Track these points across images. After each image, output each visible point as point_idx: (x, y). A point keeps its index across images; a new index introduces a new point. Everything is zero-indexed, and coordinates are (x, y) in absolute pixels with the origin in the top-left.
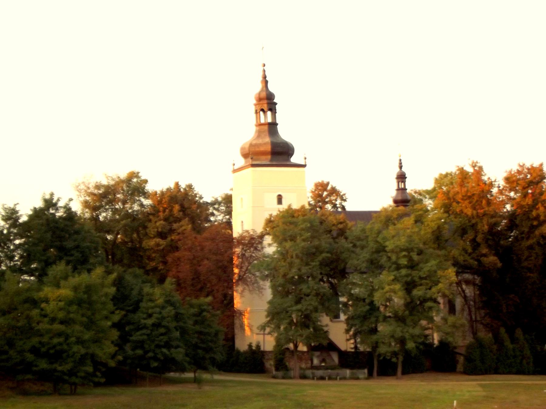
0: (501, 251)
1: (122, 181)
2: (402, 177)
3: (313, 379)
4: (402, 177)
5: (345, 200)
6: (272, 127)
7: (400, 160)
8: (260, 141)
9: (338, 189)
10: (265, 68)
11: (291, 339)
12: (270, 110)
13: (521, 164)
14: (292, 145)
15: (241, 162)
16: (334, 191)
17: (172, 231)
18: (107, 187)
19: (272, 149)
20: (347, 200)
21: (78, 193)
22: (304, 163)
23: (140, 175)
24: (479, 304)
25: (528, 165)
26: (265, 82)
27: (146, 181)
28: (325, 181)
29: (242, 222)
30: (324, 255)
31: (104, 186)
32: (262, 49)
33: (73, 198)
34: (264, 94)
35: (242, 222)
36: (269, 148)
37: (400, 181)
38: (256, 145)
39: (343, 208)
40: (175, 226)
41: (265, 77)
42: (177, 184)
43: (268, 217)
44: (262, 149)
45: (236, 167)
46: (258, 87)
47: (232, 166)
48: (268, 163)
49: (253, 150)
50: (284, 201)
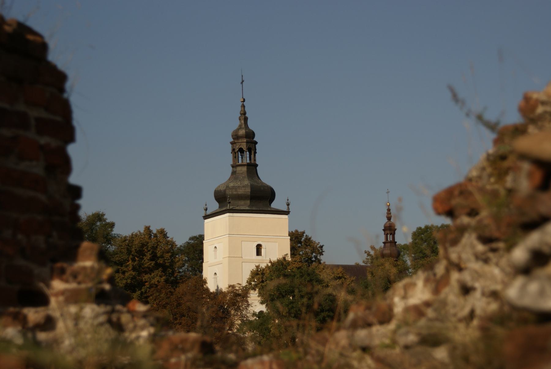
6: (252, 167)
9: (314, 240)
10: (244, 103)
20: (323, 253)
22: (285, 208)
27: (112, 225)
28: (300, 230)
32: (452, 90)
34: (242, 132)
36: (248, 190)
37: (389, 233)
40: (146, 277)
41: (244, 113)
42: (148, 229)
43: (255, 269)
44: (241, 192)
45: (209, 212)
46: (235, 124)
47: (204, 212)
48: (247, 208)
49: (230, 193)
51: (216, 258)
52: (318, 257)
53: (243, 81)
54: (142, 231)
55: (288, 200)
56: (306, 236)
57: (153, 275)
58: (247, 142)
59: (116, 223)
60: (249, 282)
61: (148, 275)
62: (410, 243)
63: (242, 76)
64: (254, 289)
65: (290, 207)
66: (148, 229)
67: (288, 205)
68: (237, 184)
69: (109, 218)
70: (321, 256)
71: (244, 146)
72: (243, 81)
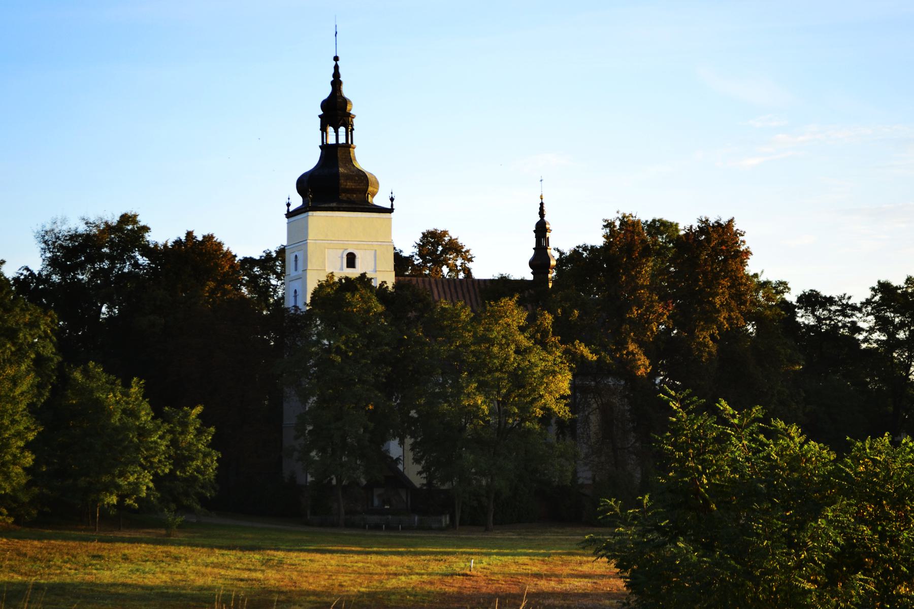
0: (198, 409)
1: (109, 228)
2: (541, 230)
3: (364, 527)
4: (541, 230)
5: (470, 260)
7: (542, 204)
11: (718, 436)
13: (473, 259)
14: (376, 178)
15: (297, 201)
16: (454, 247)
18: (87, 237)
20: (473, 259)
21: (43, 245)
22: (389, 207)
23: (138, 218)
24: (582, 433)
25: (712, 221)
26: (336, 82)
28: (440, 228)
29: (296, 291)
31: (81, 235)
33: (4, 259)
35: (296, 291)
39: (468, 272)
41: (336, 75)
42: (189, 234)
45: (292, 209)
46: (327, 91)
50: (358, 262)
51: (296, 270)
54: (183, 238)
55: (289, 199)
62: (388, 451)
63: (336, 26)
65: (394, 203)
66: (189, 234)
67: (392, 199)
69: (143, 221)
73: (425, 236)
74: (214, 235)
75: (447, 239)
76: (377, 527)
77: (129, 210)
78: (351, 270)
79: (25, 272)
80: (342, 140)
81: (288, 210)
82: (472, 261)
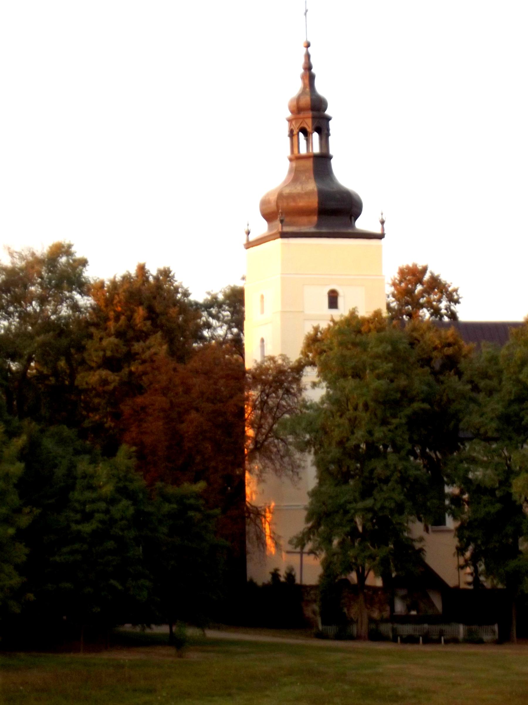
1: (39, 262)
3: (395, 640)
5: (457, 302)
8: (298, 189)
10: (309, 48)
12: (319, 130)
17: (131, 357)
19: (320, 203)
20: (460, 300)
22: (377, 230)
23: (73, 249)
27: (84, 263)
29: (262, 341)
30: (416, 405)
34: (306, 100)
35: (262, 341)
36: (314, 202)
38: (292, 197)
39: (453, 316)
40: (137, 347)
41: (308, 67)
42: (142, 269)
43: (312, 332)
44: (302, 203)
45: (252, 238)
48: (313, 230)
50: (341, 301)
52: (452, 308)
53: (307, 11)
56: (431, 273)
57: (147, 343)
58: (314, 118)
59: (332, 119)
60: (305, 354)
61: (141, 343)
63: (306, 2)
64: (312, 364)
66: (142, 269)
67: (383, 222)
68: (296, 188)
69: (79, 253)
70: (457, 304)
71: (309, 124)
72: (307, 11)
73: (403, 273)
74: (171, 269)
75: (427, 277)
76: (411, 640)
77: (64, 239)
78: (334, 312)
79: (214, 300)
80: (316, 149)
81: (248, 240)
82: (459, 303)
